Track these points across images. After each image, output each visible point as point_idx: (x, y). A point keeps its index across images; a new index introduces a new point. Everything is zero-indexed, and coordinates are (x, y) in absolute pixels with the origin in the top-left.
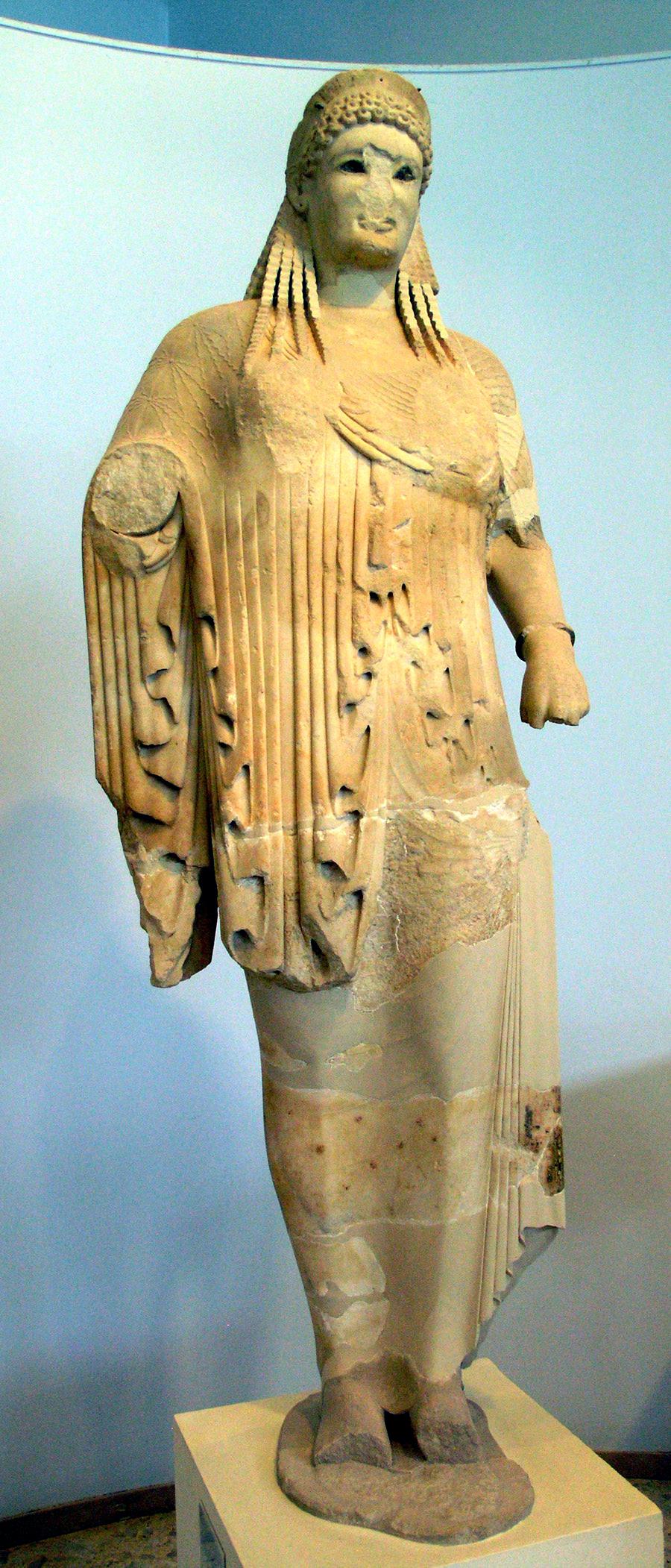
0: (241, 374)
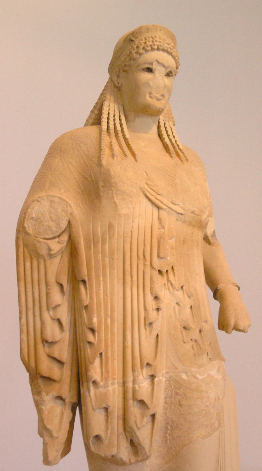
0: (99, 164)
